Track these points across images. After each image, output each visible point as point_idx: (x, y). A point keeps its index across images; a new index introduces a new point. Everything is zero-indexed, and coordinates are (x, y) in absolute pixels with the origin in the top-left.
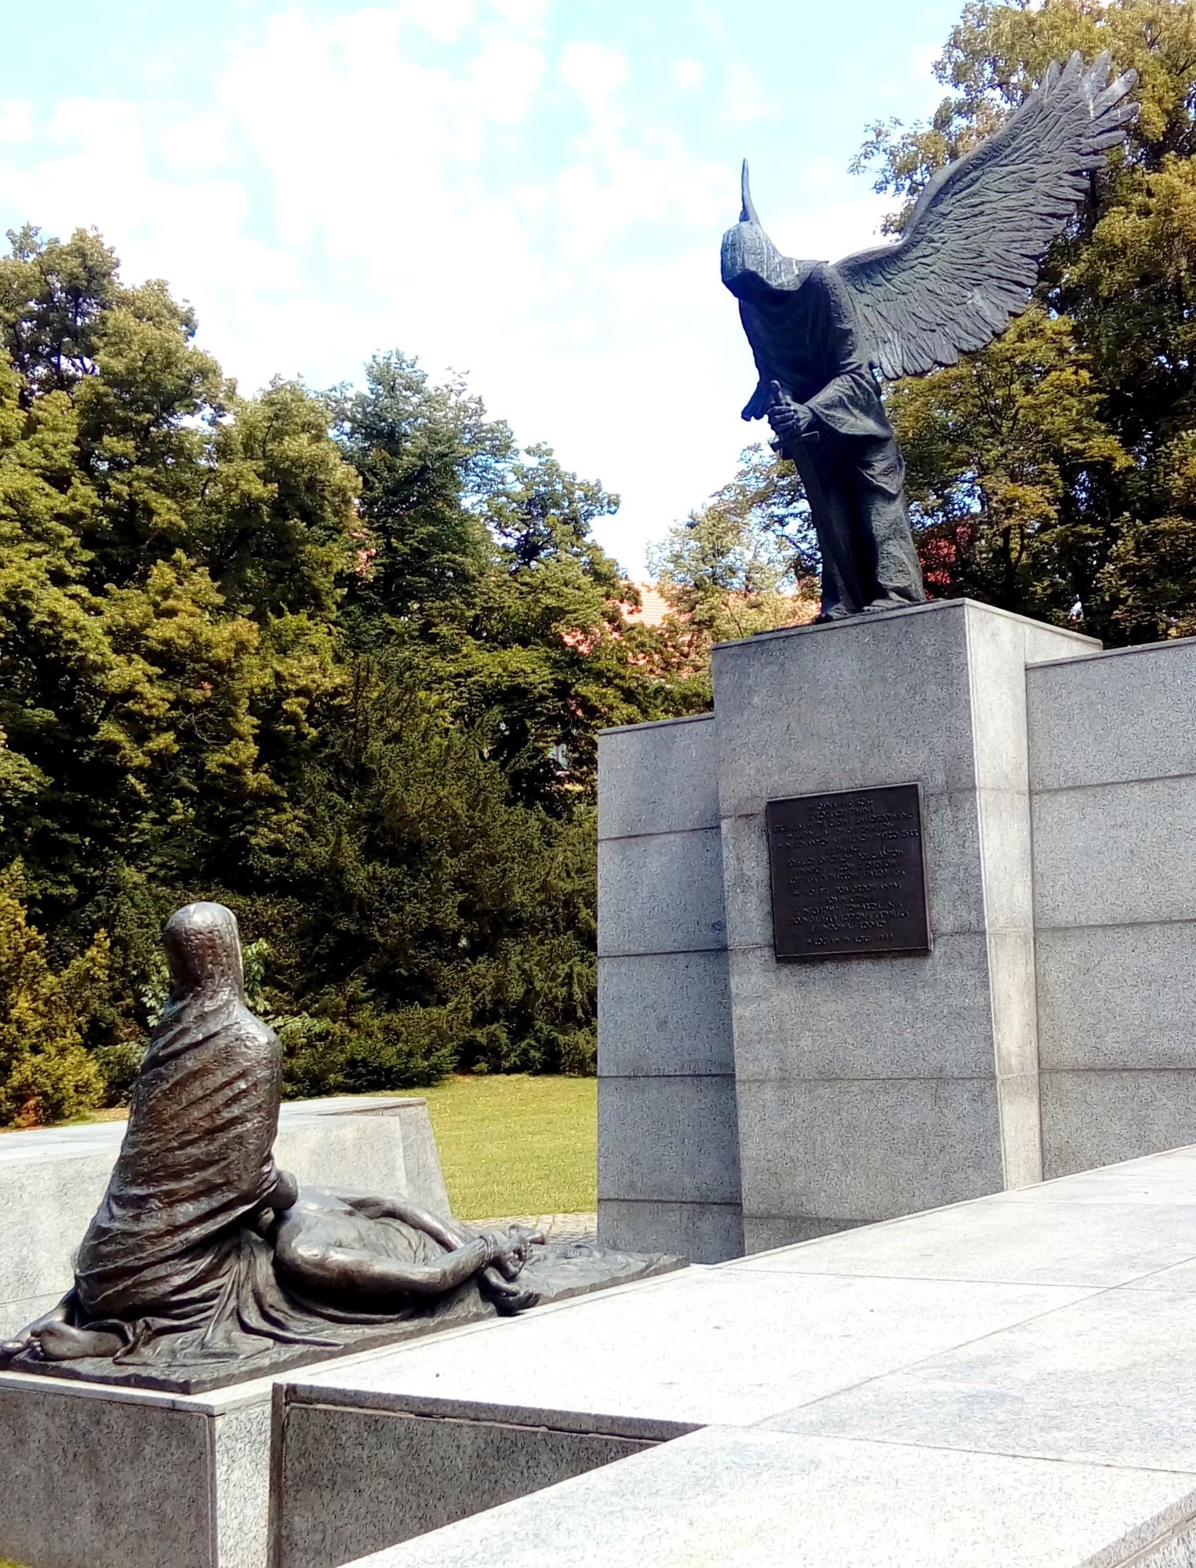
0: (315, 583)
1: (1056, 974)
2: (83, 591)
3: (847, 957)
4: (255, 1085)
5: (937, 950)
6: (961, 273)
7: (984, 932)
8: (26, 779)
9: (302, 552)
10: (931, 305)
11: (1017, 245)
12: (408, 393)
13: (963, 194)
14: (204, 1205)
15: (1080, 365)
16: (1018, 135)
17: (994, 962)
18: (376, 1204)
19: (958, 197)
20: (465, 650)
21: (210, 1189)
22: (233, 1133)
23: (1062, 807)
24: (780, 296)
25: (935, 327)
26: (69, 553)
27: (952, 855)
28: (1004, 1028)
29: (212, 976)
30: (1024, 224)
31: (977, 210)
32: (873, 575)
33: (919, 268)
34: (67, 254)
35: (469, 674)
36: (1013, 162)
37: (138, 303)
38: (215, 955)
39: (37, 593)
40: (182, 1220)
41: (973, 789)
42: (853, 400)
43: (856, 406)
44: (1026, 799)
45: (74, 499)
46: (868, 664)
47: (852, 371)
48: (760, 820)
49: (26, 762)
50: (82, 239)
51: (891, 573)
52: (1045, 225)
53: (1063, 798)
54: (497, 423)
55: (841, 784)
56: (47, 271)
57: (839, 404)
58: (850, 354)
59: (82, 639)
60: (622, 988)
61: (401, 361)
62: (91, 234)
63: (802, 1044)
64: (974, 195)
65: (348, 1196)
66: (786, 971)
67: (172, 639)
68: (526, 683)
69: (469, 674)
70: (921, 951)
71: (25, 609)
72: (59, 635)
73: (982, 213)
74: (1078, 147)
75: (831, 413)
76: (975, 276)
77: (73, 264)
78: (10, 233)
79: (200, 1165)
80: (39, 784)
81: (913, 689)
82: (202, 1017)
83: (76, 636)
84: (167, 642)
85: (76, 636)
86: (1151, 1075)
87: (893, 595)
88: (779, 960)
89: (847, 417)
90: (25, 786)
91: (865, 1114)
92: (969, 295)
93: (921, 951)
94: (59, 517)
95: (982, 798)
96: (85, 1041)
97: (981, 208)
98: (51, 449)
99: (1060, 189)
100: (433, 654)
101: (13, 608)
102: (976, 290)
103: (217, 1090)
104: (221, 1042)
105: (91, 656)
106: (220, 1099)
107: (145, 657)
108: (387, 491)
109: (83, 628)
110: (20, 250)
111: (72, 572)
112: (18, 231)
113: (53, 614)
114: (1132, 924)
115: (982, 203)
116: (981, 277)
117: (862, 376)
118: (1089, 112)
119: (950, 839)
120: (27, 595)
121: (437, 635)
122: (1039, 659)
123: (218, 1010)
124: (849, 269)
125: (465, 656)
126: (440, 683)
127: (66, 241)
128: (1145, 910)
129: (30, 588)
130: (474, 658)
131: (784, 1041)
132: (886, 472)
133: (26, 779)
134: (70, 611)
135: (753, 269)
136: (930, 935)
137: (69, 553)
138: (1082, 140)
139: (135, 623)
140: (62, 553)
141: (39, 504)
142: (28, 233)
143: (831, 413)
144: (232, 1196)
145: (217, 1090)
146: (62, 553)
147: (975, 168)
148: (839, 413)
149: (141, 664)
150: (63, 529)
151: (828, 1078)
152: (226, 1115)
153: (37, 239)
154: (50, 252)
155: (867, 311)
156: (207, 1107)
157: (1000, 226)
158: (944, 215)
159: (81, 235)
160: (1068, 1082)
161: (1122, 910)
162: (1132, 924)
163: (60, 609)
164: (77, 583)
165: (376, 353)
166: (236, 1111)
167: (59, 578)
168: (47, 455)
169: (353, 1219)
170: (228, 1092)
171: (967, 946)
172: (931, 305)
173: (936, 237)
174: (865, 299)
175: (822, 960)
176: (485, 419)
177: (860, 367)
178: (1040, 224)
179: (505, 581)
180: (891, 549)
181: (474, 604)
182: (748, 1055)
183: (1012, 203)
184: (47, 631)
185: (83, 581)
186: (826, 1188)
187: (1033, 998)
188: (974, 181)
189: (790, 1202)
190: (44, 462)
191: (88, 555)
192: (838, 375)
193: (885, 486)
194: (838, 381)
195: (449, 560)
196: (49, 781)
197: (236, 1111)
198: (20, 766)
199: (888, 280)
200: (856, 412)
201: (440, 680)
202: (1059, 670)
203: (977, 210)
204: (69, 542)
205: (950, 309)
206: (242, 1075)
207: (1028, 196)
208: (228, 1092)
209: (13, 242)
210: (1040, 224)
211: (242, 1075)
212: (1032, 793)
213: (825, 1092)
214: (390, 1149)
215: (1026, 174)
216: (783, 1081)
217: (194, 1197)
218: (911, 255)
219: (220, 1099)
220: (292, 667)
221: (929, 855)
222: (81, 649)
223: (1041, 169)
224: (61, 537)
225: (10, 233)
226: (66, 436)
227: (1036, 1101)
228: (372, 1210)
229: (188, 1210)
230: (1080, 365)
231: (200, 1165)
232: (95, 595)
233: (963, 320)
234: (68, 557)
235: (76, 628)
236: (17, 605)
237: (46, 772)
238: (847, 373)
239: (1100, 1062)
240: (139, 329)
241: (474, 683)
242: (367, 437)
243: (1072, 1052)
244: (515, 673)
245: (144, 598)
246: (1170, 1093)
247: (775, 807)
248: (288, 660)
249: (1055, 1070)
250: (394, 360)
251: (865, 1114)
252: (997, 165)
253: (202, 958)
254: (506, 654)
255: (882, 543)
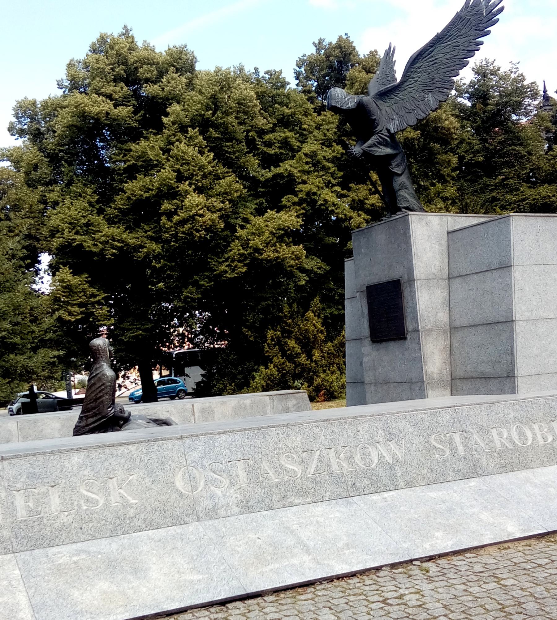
0: (442, 172)
1: (456, 344)
2: (338, 189)
3: (387, 340)
4: (106, 387)
5: (409, 337)
6: (425, 88)
7: (418, 331)
8: (319, 268)
9: (437, 158)
10: (412, 102)
11: (448, 73)
12: (493, 77)
13: (427, 57)
14: (95, 419)
15: (307, 163)
16: (450, 30)
17: (424, 341)
18: (161, 420)
19: (425, 59)
20: (522, 189)
21: (95, 415)
22: (101, 400)
23: (456, 283)
24: (349, 111)
25: (411, 111)
26: (332, 174)
27: (410, 304)
28: (429, 364)
29: (99, 358)
30: (452, 64)
32: (396, 203)
33: (409, 89)
34: (334, 48)
35: (524, 200)
37: (364, 63)
38: (99, 352)
39: (318, 192)
40: (89, 423)
41: (414, 280)
42: (380, 143)
43: (381, 145)
44: (447, 281)
45: (334, 151)
47: (378, 133)
49: (319, 261)
50: (340, 41)
52: (461, 63)
54: (532, 84)
55: (384, 279)
56: (327, 57)
57: (374, 145)
58: (376, 127)
59: (336, 209)
61: (487, 62)
62: (344, 37)
64: (432, 57)
67: (374, 204)
68: (550, 201)
69: (524, 200)
70: (405, 338)
71: (314, 199)
72: (327, 208)
73: (436, 63)
74: (478, 28)
75: (371, 149)
76: (430, 88)
77: (337, 52)
78: (314, 43)
79: (94, 408)
80: (325, 269)
82: (96, 369)
83: (333, 208)
84: (373, 205)
85: (333, 208)
86: (478, 380)
87: (403, 210)
89: (378, 149)
90: (319, 271)
92: (427, 96)
94: (328, 160)
95: (417, 284)
97: (435, 61)
98: (326, 132)
99: (471, 47)
100: (507, 193)
101: (309, 200)
102: (430, 94)
103: (97, 389)
104: (99, 376)
105: (340, 216)
106: (98, 391)
107: (365, 213)
108: (483, 122)
109: (337, 204)
110: (318, 49)
111: (334, 182)
112: (317, 42)
113: (325, 200)
114: (474, 326)
116: (431, 88)
117: (383, 134)
118: (483, 14)
119: (409, 298)
120: (315, 194)
121: (508, 184)
122: (451, 229)
123: (100, 367)
124: (379, 95)
125: (522, 192)
126: (510, 206)
127: (334, 42)
128: (477, 321)
129: (315, 191)
130: (526, 193)
132: (397, 166)
133: (319, 268)
134: (331, 198)
135: (334, 105)
136: (406, 332)
137: (332, 174)
138: (480, 25)
139: (361, 198)
140: (329, 175)
141: (321, 155)
142: (321, 41)
143: (371, 149)
144: (100, 416)
145: (97, 389)
146: (329, 175)
147: (431, 47)
148: (374, 149)
149: (364, 215)
150: (330, 165)
151: (386, 383)
152: (99, 395)
153: (324, 44)
154: (329, 48)
155: (387, 109)
156: (95, 393)
157: (442, 67)
158: (419, 68)
159: (340, 39)
160: (458, 382)
161: (471, 320)
162: (474, 326)
163: (327, 198)
164: (336, 186)
165: (476, 61)
166: (101, 394)
167: (328, 184)
168: (325, 135)
170: (100, 389)
172: (412, 102)
174: (387, 104)
176: (525, 83)
177: (381, 131)
179: (541, 155)
180: (402, 193)
181: (526, 168)
184: (322, 207)
185: (338, 184)
187: (448, 353)
188: (432, 52)
190: (323, 138)
191: (341, 174)
192: (374, 135)
193: (396, 171)
194: (373, 137)
195: (512, 149)
196: (328, 268)
197: (101, 394)
198: (317, 263)
199: (396, 96)
200: (381, 147)
201: (510, 204)
202: (456, 233)
204: (332, 170)
205: (418, 103)
206: (103, 385)
207: (455, 53)
208: (100, 389)
209: (316, 47)
211: (103, 385)
212: (449, 279)
213: (385, 387)
214: (265, 407)
215: (455, 44)
216: (376, 384)
217: (92, 417)
218: (405, 85)
219: (98, 391)
220: (432, 208)
221: (405, 304)
222: (336, 213)
224: (329, 168)
225: (314, 43)
226: (332, 125)
227: (449, 390)
228: (160, 422)
229: (91, 420)
230: (307, 163)
231: (94, 408)
232: (342, 189)
233: (422, 107)
234: (332, 176)
235: (334, 205)
236: (311, 198)
237: (328, 265)
238: (376, 134)
239: (466, 376)
240: (359, 76)
241: (527, 204)
242: (477, 98)
243: (459, 373)
244: (545, 197)
245: (366, 187)
246: (483, 386)
247: (368, 287)
248: (430, 206)
249: (455, 379)
250: (484, 63)
252: (443, 43)
253: (96, 353)
254: (541, 189)
255: (397, 192)
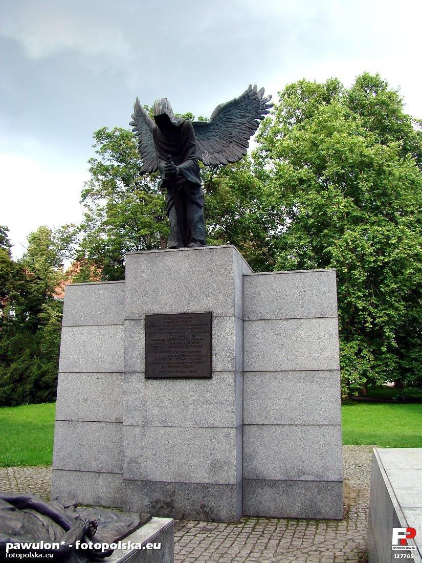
31: (230, 120)
33: (214, 133)
36: (240, 109)
46: (193, 265)
47: (193, 159)
48: (143, 322)
51: (198, 234)
53: (256, 323)
55: (178, 309)
60: (69, 385)
63: (153, 412)
65: (8, 497)
66: (149, 382)
73: (231, 122)
81: (211, 277)
88: (146, 378)
91: (179, 441)
93: (209, 377)
96: (348, 340)
115: (231, 119)
131: (145, 411)
169: (14, 513)
171: (226, 376)
173: (219, 124)
175: (165, 378)
178: (248, 130)
182: (129, 415)
183: (240, 121)
186: (160, 469)
189: (143, 475)
203: (230, 120)
210: (248, 130)
215: (244, 114)
223: (247, 114)
251: (179, 441)
252: (236, 108)
